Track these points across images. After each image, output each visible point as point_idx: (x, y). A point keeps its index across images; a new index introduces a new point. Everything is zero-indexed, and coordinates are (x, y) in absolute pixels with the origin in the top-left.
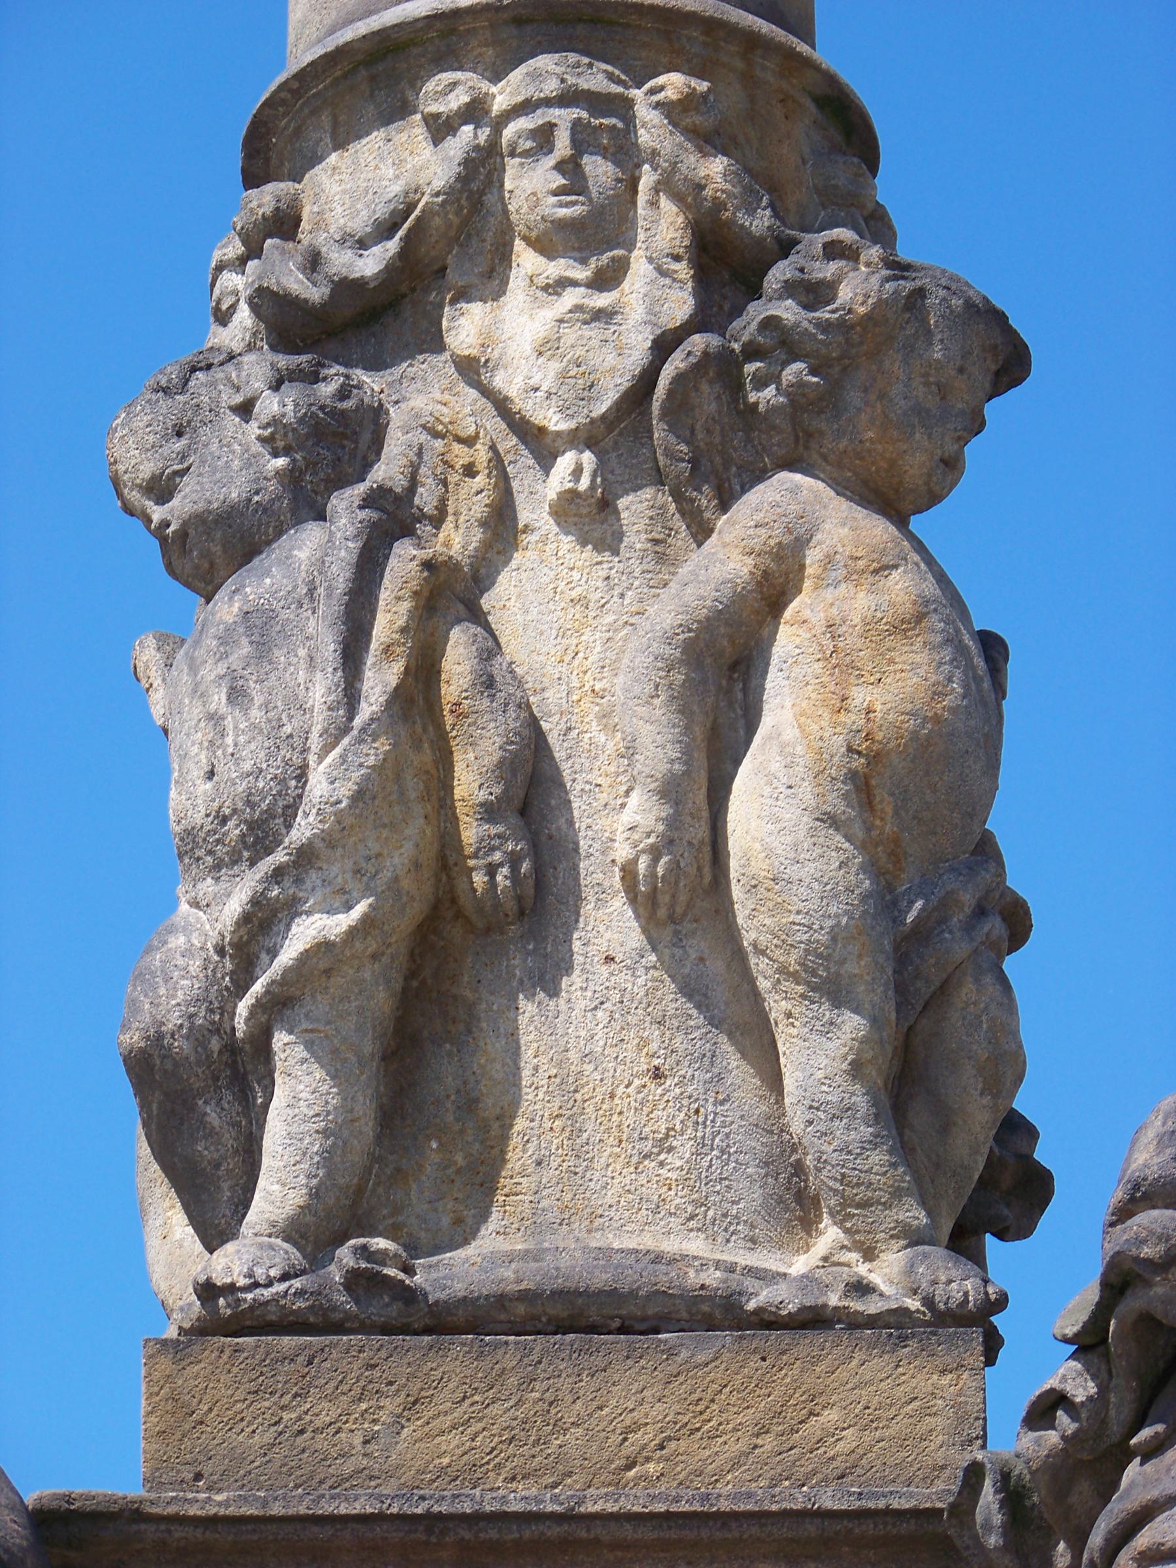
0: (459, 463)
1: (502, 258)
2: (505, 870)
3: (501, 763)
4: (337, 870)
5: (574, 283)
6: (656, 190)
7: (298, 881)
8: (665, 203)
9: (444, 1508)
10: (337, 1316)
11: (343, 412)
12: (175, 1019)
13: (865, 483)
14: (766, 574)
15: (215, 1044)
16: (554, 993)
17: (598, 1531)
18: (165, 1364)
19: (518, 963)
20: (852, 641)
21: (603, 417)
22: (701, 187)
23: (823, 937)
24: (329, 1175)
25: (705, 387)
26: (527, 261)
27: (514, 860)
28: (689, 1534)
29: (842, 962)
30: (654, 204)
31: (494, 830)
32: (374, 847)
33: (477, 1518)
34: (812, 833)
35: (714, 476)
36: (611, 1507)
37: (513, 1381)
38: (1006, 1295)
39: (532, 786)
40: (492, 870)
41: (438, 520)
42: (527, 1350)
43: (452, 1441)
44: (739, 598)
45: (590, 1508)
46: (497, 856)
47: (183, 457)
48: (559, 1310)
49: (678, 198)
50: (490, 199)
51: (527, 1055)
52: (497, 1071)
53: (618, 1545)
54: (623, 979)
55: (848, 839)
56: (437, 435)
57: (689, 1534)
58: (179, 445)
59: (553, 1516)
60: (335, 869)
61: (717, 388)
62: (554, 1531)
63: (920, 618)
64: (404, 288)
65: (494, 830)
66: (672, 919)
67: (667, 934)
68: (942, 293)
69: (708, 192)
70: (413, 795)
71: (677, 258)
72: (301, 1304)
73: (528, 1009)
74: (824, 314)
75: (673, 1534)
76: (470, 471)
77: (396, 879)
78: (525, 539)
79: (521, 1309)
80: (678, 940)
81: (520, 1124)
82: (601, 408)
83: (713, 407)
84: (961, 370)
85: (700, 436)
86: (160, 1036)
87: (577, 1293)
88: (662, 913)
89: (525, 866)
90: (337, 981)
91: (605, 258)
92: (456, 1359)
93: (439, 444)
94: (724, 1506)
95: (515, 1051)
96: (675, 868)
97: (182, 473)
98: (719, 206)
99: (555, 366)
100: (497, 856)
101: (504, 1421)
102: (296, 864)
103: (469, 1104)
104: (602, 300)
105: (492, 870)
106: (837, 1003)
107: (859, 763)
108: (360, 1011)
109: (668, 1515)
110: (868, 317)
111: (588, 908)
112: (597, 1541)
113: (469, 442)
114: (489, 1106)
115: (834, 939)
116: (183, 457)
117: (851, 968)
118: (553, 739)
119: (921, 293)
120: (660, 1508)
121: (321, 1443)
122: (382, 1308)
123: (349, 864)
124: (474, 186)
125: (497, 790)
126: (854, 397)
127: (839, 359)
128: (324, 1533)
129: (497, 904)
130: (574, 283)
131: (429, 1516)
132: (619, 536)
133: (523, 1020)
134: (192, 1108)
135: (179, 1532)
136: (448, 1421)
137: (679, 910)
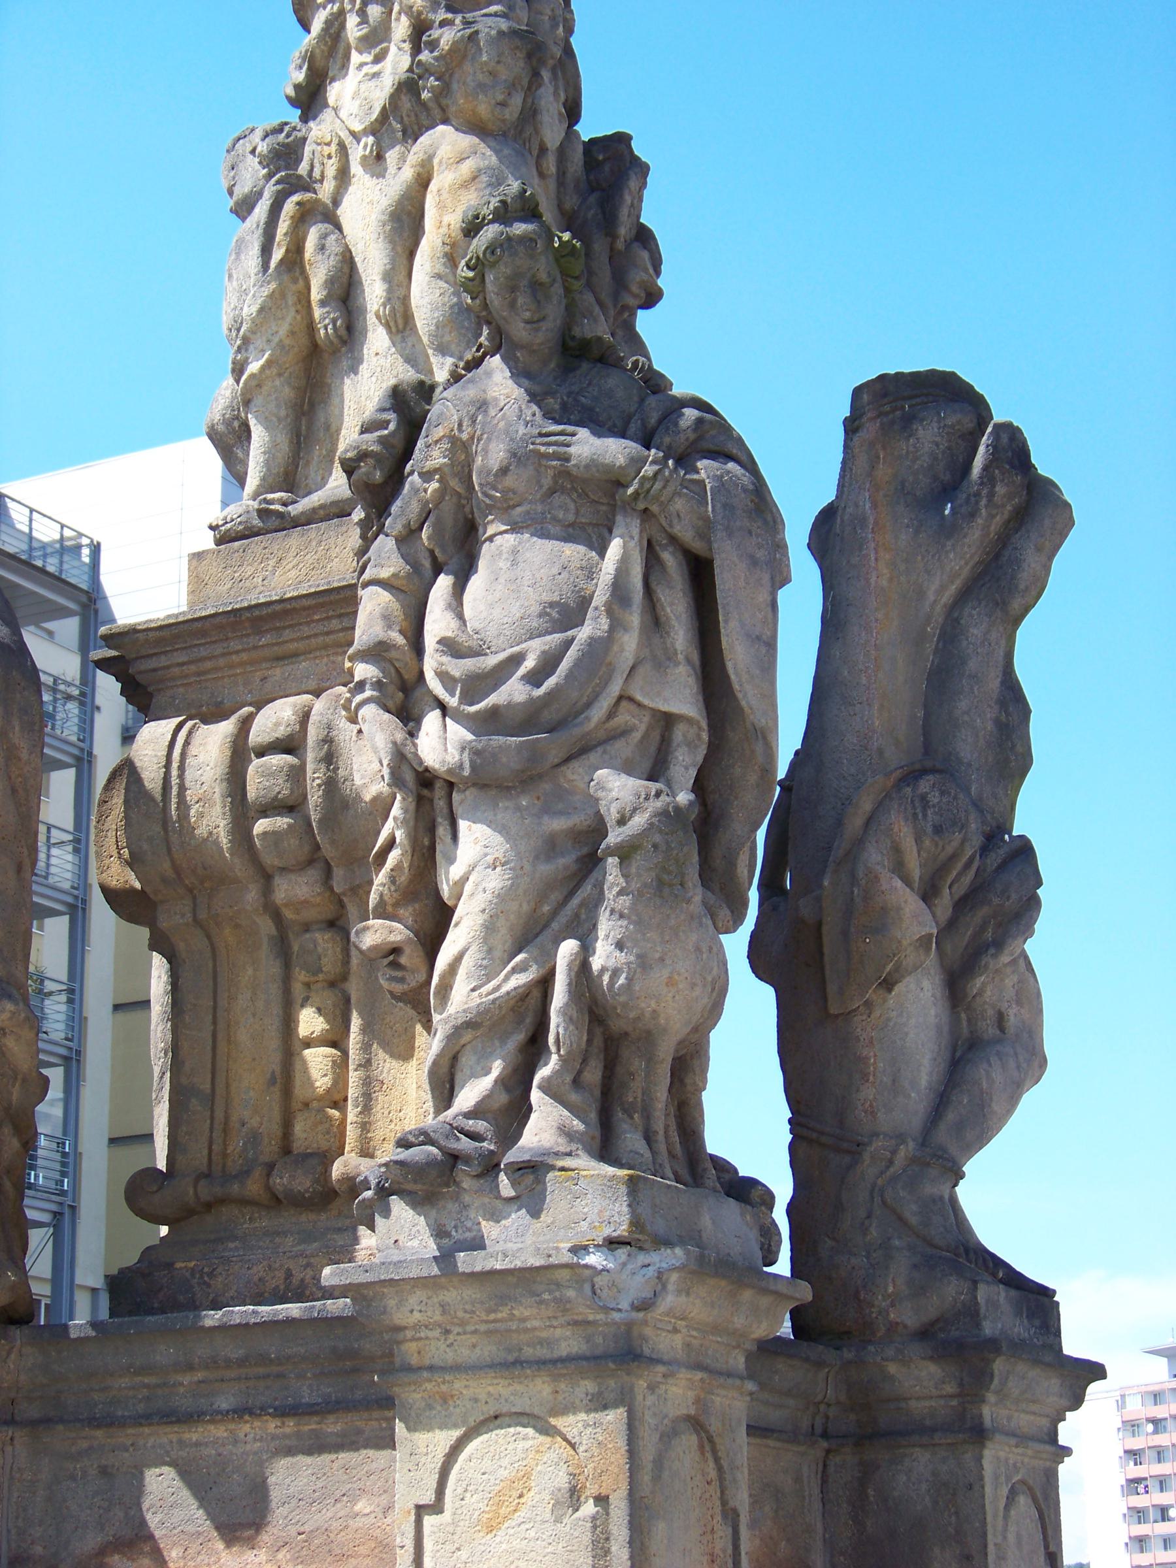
0: (326, 154)
1: (347, 57)
2: (330, 327)
3: (326, 281)
4: (259, 342)
5: (366, 64)
6: (400, 13)
7: (246, 350)
8: (404, 18)
9: (237, 606)
10: (256, 530)
11: (288, 144)
12: (217, 417)
13: (469, 122)
14: (419, 174)
15: (236, 424)
16: (356, 373)
17: (294, 604)
18: (195, 562)
19: (345, 364)
20: (445, 195)
21: (376, 120)
22: (412, 7)
23: (433, 328)
24: (268, 470)
25: (403, 97)
26: (356, 58)
27: (334, 321)
28: (326, 599)
29: (442, 336)
30: (398, 19)
31: (325, 310)
32: (274, 329)
33: (250, 608)
34: (429, 283)
35: (412, 134)
36: (295, 594)
37: (314, 543)
38: (943, 392)
39: (346, 288)
40: (326, 328)
41: (321, 181)
42: (319, 529)
43: (294, 573)
44: (409, 188)
45: (288, 595)
46: (327, 321)
47: (234, 178)
48: (334, 510)
49: (406, 14)
50: (343, 35)
51: (346, 402)
52: (336, 412)
53: (304, 609)
54: (382, 361)
55: (446, 282)
56: (319, 144)
57: (326, 599)
58: (232, 173)
59: (276, 601)
60: (259, 342)
61: (409, 96)
62: (278, 607)
63: (474, 178)
64: (318, 82)
65: (325, 310)
66: (398, 331)
67: (398, 338)
68: (487, 30)
69: (415, 9)
70: (290, 303)
71: (404, 41)
72: (241, 527)
73: (347, 381)
74: (436, 54)
75: (321, 600)
76: (330, 157)
77: (281, 341)
78: (353, 180)
79: (322, 512)
80: (403, 340)
81: (343, 432)
82: (374, 116)
83: (409, 105)
84: (498, 62)
85: (405, 119)
86: (213, 426)
87: (339, 502)
88: (394, 329)
89: (339, 323)
90: (265, 389)
91: (378, 49)
92: (294, 539)
93: (319, 148)
94: (336, 585)
95: (342, 401)
96: (393, 310)
97: (234, 185)
98: (420, 13)
99: (358, 102)
100: (327, 321)
101: (310, 561)
102: (244, 343)
103: (328, 427)
104: (376, 68)
105: (326, 328)
106: (444, 355)
107: (447, 248)
108: (276, 399)
109: (316, 593)
110: (450, 50)
111: (370, 334)
112: (294, 609)
113: (328, 144)
114: (333, 428)
115: (437, 328)
116: (234, 178)
117: (447, 338)
118: (359, 265)
119: (477, 32)
120: (313, 590)
121: (248, 584)
122: (274, 522)
123: (264, 339)
124: (332, 31)
125: (324, 293)
126: (455, 86)
127: (447, 71)
128: (199, 625)
129: (331, 343)
130: (366, 64)
131: (233, 611)
132: (386, 170)
133: (346, 387)
134: (232, 452)
135: (151, 634)
136: (291, 565)
137: (401, 327)
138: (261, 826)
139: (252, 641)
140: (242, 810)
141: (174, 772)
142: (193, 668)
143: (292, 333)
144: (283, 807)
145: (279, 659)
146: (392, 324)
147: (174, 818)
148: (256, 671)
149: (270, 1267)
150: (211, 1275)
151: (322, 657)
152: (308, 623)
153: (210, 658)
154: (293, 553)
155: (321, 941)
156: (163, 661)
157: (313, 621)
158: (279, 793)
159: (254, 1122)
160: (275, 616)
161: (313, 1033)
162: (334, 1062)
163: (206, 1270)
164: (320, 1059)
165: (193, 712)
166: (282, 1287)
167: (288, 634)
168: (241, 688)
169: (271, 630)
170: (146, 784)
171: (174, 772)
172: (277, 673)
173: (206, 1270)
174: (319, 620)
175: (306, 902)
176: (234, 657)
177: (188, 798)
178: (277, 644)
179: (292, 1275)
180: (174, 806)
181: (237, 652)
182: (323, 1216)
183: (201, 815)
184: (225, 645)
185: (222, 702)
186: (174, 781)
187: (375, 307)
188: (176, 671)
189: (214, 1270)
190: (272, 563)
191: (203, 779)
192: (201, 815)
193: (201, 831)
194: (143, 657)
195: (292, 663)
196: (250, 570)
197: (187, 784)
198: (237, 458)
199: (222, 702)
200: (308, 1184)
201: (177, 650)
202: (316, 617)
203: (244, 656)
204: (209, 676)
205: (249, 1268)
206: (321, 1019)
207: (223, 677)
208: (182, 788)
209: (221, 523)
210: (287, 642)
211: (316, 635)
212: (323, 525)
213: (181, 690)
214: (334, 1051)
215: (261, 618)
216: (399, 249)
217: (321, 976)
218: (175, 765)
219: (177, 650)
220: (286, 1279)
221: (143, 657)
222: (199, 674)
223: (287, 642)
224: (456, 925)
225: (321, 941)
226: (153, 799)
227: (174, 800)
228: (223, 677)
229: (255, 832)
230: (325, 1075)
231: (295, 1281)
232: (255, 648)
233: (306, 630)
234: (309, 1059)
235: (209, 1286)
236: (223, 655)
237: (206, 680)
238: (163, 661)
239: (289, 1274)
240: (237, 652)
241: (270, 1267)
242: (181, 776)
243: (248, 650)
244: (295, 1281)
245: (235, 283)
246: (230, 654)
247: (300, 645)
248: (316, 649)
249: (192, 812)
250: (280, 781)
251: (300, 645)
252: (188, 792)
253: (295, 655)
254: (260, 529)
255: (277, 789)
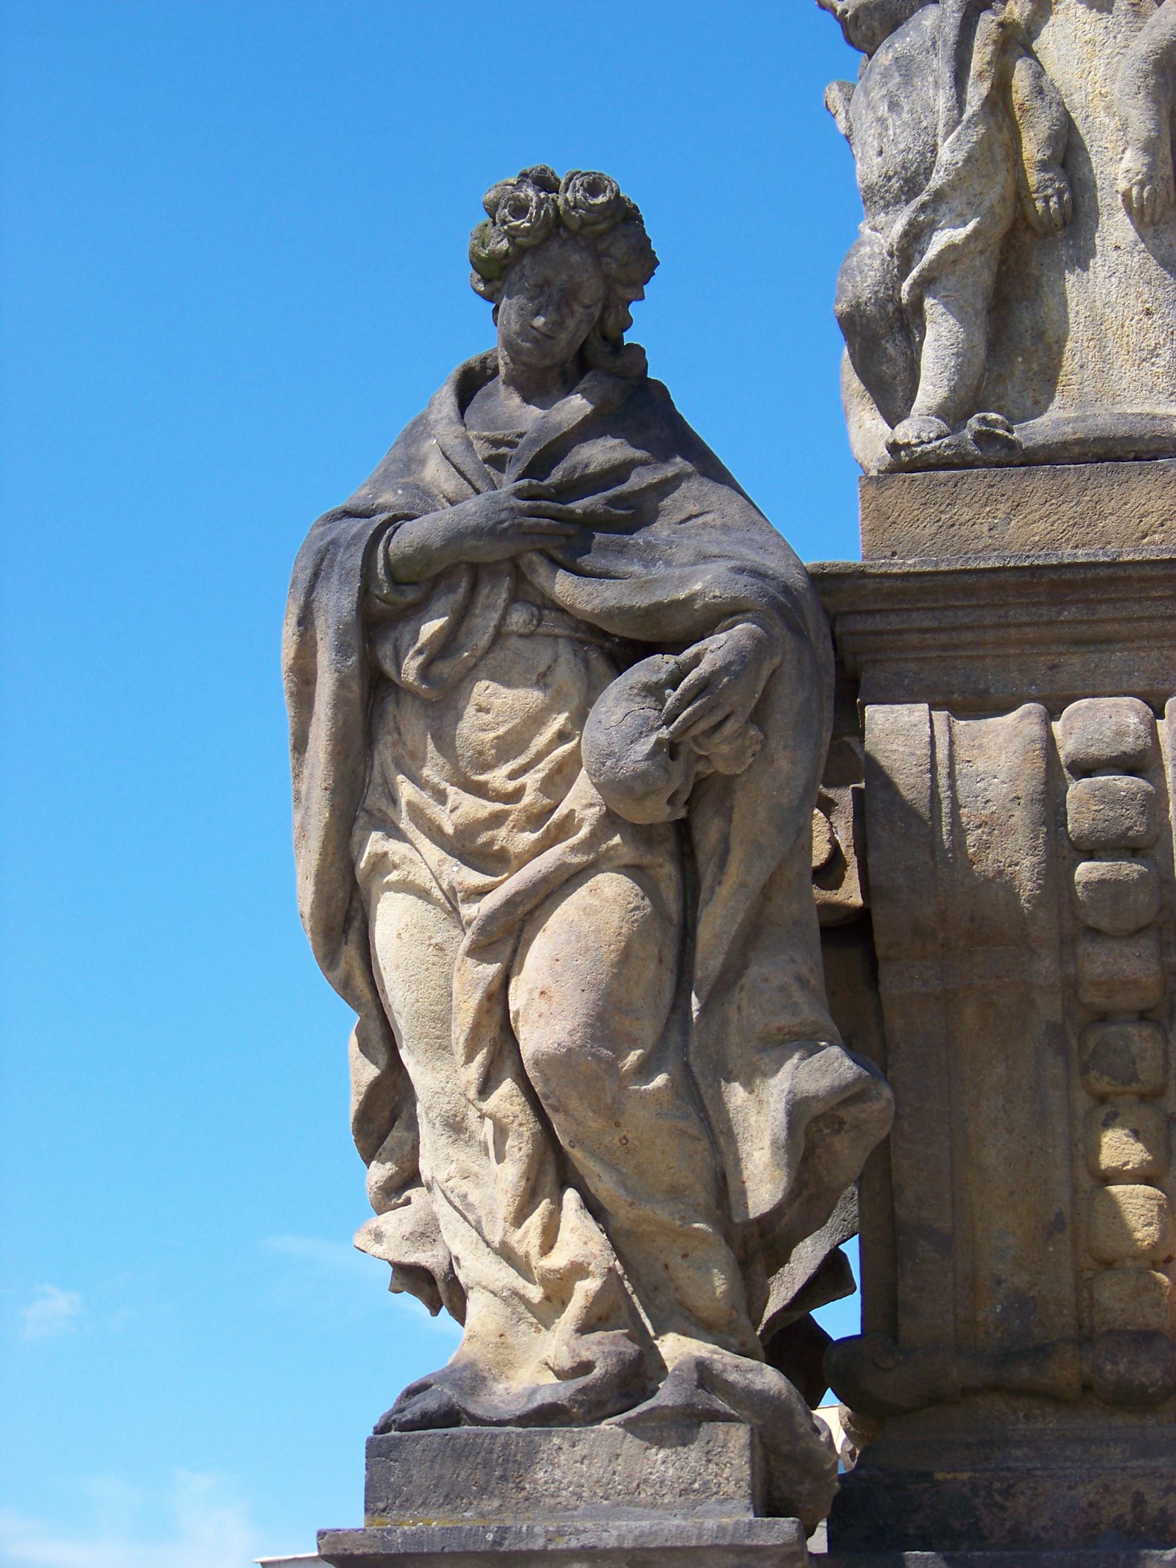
3: (1049, 137)
7: (935, 211)
10: (970, 458)
12: (867, 294)
16: (1085, 268)
17: (1131, 571)
19: (1064, 253)
24: (961, 379)
27: (1059, 193)
36: (1138, 557)
37: (1074, 490)
40: (1047, 200)
43: (1041, 526)
46: (1050, 191)
51: (1072, 305)
53: (1142, 580)
54: (1125, 258)
60: (956, 202)
62: (1104, 573)
66: (1153, 223)
70: (999, 158)
73: (1071, 279)
77: (992, 207)
79: (1076, 450)
81: (1069, 345)
86: (858, 305)
87: (1109, 439)
88: (1147, 219)
89: (1066, 197)
96: (1153, 192)
100: (1050, 191)
101: (1070, 514)
105: (1047, 200)
111: (1103, 219)
114: (1051, 336)
120: (1167, 556)
123: (964, 199)
125: (1048, 153)
129: (1051, 219)
131: (1031, 567)
133: (1068, 285)
136: (1037, 516)
137: (1157, 217)
138: (1085, 871)
139: (1046, 613)
140: (1062, 848)
141: (943, 781)
142: (943, 638)
143: (1003, 198)
144: (1126, 848)
145: (1080, 642)
146: (1148, 211)
147: (947, 845)
148: (1041, 654)
149: (1106, 1488)
150: (1006, 1493)
151: (1151, 649)
152: (1139, 601)
153: (969, 628)
154: (1035, 502)
155: (1136, 1038)
156: (876, 623)
157: (1147, 599)
158: (1130, 828)
159: (1021, 1280)
160: (1096, 583)
161: (1126, 1163)
162: (1160, 1206)
163: (997, 1485)
164: (1141, 1201)
165: (939, 699)
166: (1129, 1517)
167: (1104, 611)
168: (1015, 675)
169: (1078, 602)
170: (904, 793)
171: (943, 781)
172: (1075, 662)
173: (997, 1485)
174: (1160, 598)
175: (1135, 982)
176: (1013, 631)
177: (964, 819)
178: (1088, 622)
179: (1145, 1502)
180: (945, 829)
181: (1019, 625)
182: (1151, 1421)
183: (985, 846)
184: (1001, 612)
185: (986, 691)
186: (944, 793)
187: (1122, 185)
188: (914, 639)
189: (1010, 1486)
190: (1003, 508)
191: (989, 795)
192: (985, 846)
193: (986, 865)
194: (860, 613)
195: (1101, 651)
196: (967, 514)
197: (961, 800)
198: (885, 354)
199: (986, 691)
200: (1158, 1374)
201: (918, 609)
202: (1154, 594)
203: (1030, 632)
204: (962, 653)
205: (1070, 1488)
206: (1140, 1146)
207: (984, 657)
208: (955, 805)
209: (914, 441)
210: (1103, 621)
211: (1151, 618)
212: (1088, 468)
213: (912, 666)
214: (1149, 1190)
215: (1071, 585)
216: (1164, 112)
217: (1135, 1086)
218: (942, 771)
219: (918, 609)
220: (1134, 1507)
221: (860, 613)
222: (945, 648)
223: (1103, 621)
224: (516, 1021)
225: (1136, 1038)
226: (916, 814)
227: (946, 820)
228: (984, 657)
229: (1077, 878)
230: (1150, 1224)
231: (1152, 1509)
232: (1051, 623)
233: (1136, 610)
234: (1122, 1199)
235: (1003, 1508)
236: (997, 626)
237: (955, 658)
238: (894, 622)
239: (1139, 1500)
240: (1019, 625)
241: (1106, 1488)
242: (952, 787)
243: (1037, 624)
244: (1152, 1509)
245: (906, 116)
246: (1009, 626)
247: (1124, 629)
248: (1148, 637)
249: (970, 840)
250: (1132, 812)
251: (1124, 629)
252: (962, 811)
253: (1109, 640)
254: (976, 458)
255: (1128, 823)
